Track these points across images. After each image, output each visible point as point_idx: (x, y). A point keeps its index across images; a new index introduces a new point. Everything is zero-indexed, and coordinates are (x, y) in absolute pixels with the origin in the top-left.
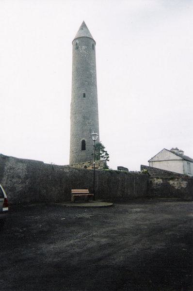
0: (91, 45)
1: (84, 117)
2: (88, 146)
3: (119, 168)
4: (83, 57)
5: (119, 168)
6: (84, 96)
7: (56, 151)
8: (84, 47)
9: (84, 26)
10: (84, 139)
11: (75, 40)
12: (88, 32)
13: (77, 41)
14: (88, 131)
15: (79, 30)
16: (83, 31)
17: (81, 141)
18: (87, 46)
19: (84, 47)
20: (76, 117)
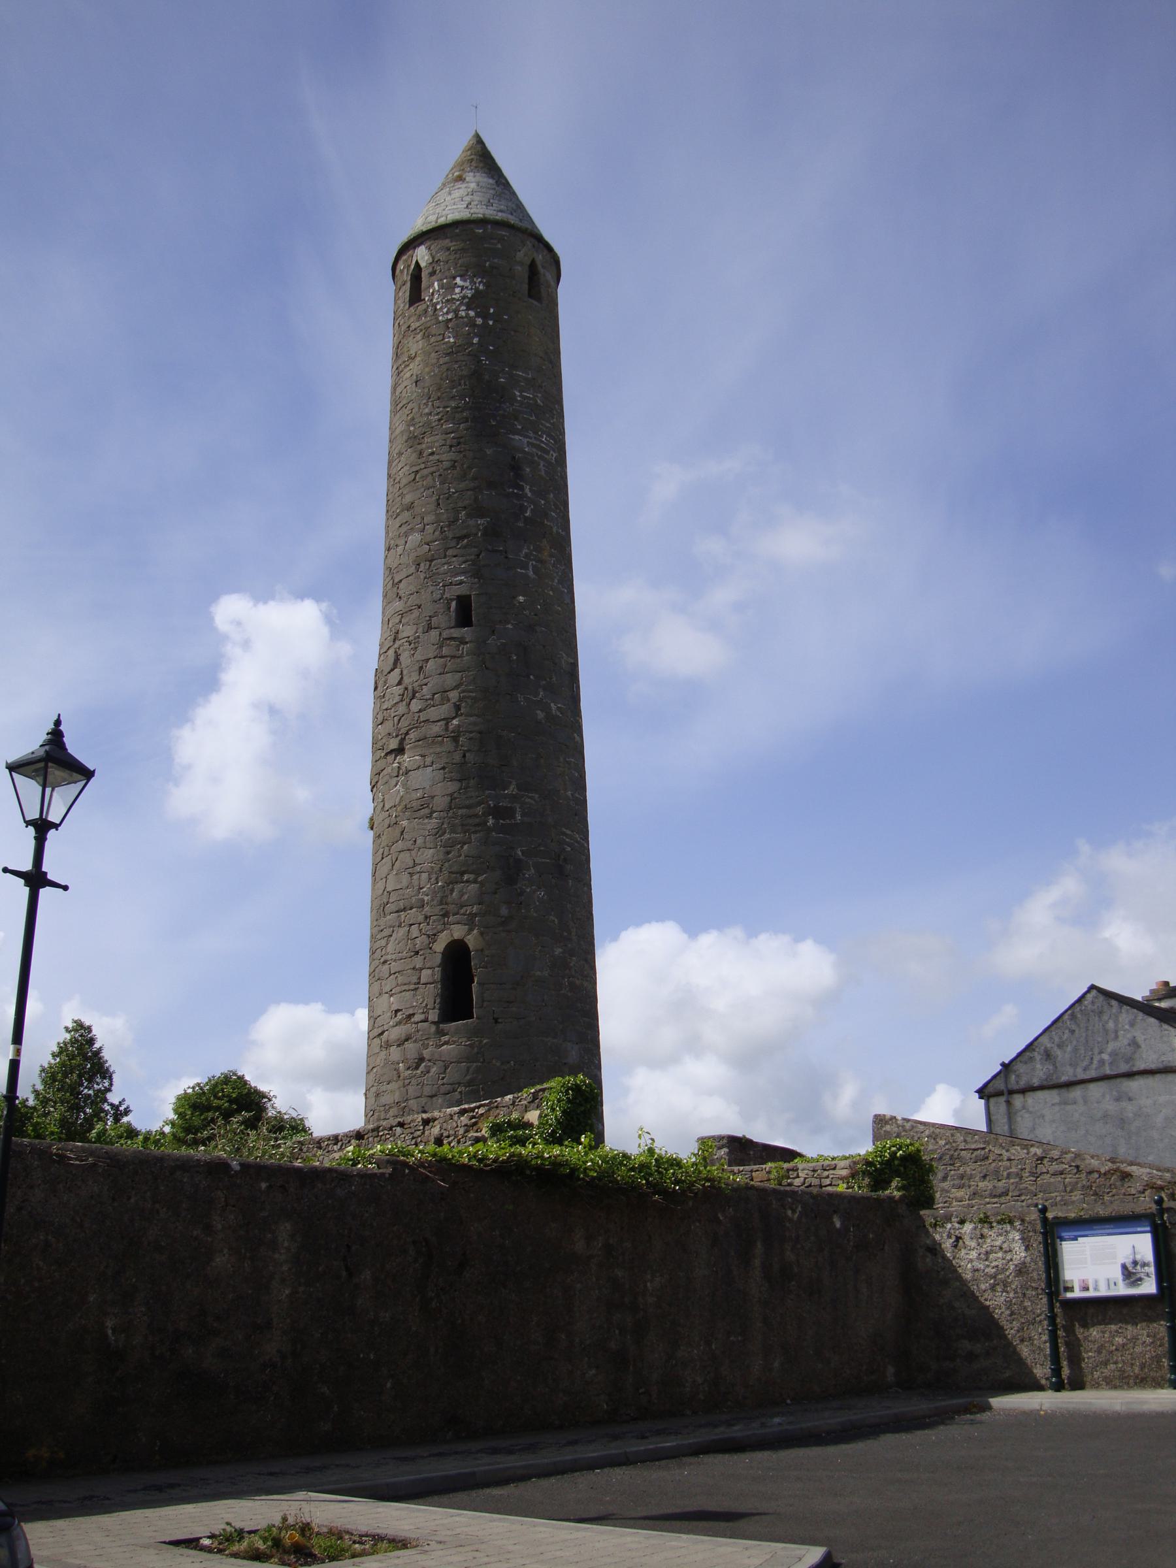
0: (521, 271)
9: (481, 158)
16: (460, 191)
17: (440, 946)
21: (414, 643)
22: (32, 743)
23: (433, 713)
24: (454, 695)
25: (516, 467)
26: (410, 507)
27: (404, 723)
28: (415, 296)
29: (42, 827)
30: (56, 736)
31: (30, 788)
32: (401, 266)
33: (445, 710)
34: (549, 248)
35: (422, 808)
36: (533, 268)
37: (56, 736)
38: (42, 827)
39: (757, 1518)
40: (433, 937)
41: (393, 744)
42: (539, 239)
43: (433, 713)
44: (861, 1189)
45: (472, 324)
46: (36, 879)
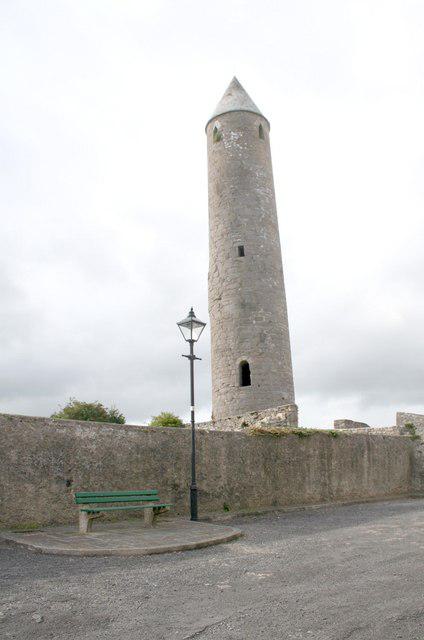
0: (256, 129)
1: (243, 305)
2: (256, 357)
3: (337, 424)
4: (233, 159)
5: (337, 424)
6: (242, 252)
7: (204, 408)
8: (241, 142)
9: (236, 85)
10: (244, 358)
11: (210, 121)
12: (246, 98)
13: (217, 124)
14: (258, 339)
15: (224, 98)
16: (231, 99)
17: (238, 362)
18: (245, 130)
19: (241, 142)
20: (221, 307)
21: (223, 263)
22: (184, 316)
23: (231, 286)
24: (239, 280)
25: (258, 199)
26: (218, 215)
27: (220, 291)
28: (219, 139)
29: (192, 342)
30: (192, 314)
31: (186, 331)
32: (209, 128)
33: (235, 285)
34: (266, 120)
35: (229, 318)
36: (260, 128)
37: (192, 314)
38: (192, 342)
39: (215, 548)
40: (235, 360)
41: (217, 297)
42: (261, 116)
43: (231, 286)
44: (397, 434)
45: (238, 149)
46: (192, 358)
